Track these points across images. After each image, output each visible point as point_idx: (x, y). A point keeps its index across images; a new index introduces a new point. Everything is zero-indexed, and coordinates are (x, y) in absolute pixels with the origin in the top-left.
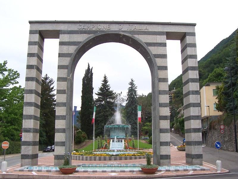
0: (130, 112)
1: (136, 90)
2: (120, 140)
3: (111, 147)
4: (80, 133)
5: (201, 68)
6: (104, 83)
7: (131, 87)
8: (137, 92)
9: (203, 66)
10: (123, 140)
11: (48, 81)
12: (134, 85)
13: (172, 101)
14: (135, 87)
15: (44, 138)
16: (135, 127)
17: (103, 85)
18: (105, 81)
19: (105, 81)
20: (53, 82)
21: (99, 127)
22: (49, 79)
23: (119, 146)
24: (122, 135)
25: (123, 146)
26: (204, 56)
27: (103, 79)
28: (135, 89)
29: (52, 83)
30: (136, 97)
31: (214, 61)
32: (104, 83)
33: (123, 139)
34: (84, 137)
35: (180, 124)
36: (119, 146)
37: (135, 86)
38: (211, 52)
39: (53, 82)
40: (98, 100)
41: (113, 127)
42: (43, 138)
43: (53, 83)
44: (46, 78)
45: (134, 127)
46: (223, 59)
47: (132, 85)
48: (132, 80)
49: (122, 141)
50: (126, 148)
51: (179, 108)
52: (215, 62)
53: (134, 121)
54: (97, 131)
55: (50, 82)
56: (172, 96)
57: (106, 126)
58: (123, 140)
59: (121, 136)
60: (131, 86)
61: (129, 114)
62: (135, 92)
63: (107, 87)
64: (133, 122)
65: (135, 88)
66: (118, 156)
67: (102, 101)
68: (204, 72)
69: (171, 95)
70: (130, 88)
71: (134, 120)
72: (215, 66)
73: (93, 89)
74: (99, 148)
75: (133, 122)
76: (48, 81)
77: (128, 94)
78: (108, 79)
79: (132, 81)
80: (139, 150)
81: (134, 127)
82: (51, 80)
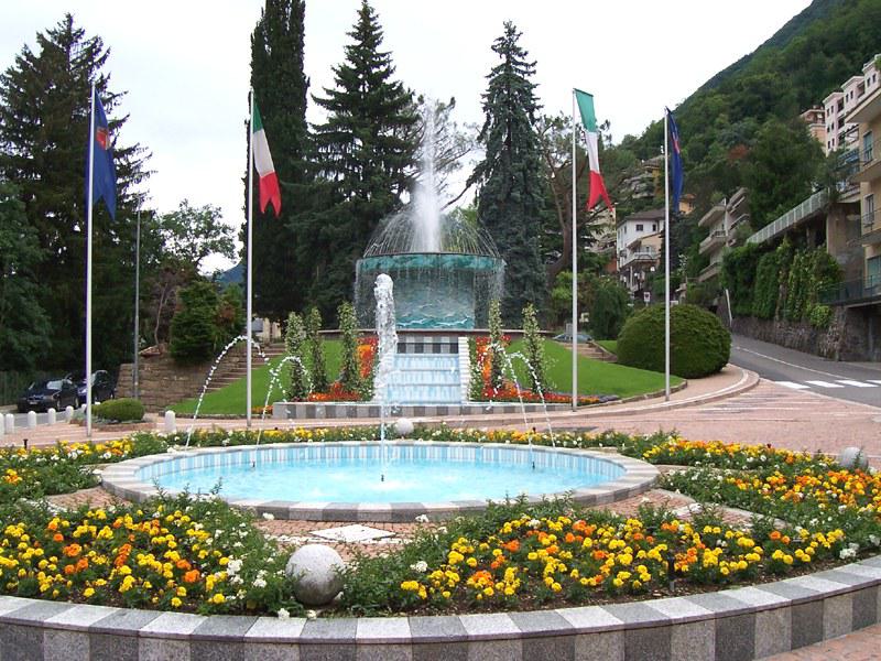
0: (501, 197)
1: (532, 79)
2: (446, 340)
3: (380, 382)
4: (200, 300)
5: (770, 71)
6: (358, 43)
7: (507, 66)
8: (533, 91)
9: (779, 63)
10: (463, 341)
11: (76, 52)
12: (520, 55)
13: (652, 197)
14: (527, 65)
15: (35, 333)
16: (525, 277)
17: (354, 54)
18: (367, 32)
19: (367, 32)
20: (101, 55)
21: (332, 276)
22: (85, 38)
23: (439, 379)
24: (456, 312)
25: (466, 377)
26: (798, 13)
27: (356, 20)
28: (526, 77)
29: (97, 59)
30: (531, 116)
31: (823, 42)
32: (358, 43)
33: (463, 334)
34: (227, 321)
35: (734, 274)
36: (439, 379)
37: (528, 60)
38: (768, 43)
39: (101, 55)
40: (330, 135)
41: (403, 271)
42: (30, 338)
43: (103, 60)
44: (65, 37)
45: (519, 275)
46: (862, 34)
47: (508, 57)
48: (507, 26)
49: (454, 348)
50: (350, 301)
51: (711, 208)
52: (827, 45)
53: (519, 243)
54: (322, 297)
55: (92, 51)
56: (652, 180)
57: (364, 261)
58: (463, 341)
59: (452, 319)
60: (504, 60)
61: (494, 207)
62: (526, 91)
63: (376, 29)
64: (515, 248)
65: (523, 73)
66: (397, 604)
67: (349, 139)
68: (782, 86)
69: (650, 175)
70: (496, 70)
71: (520, 235)
72: (828, 60)
73: (308, 85)
74: (297, 393)
75: (515, 248)
76: (76, 52)
77: (486, 100)
78: (385, 21)
79: (511, 32)
80: (582, 404)
81: (519, 275)
82: (94, 46)
